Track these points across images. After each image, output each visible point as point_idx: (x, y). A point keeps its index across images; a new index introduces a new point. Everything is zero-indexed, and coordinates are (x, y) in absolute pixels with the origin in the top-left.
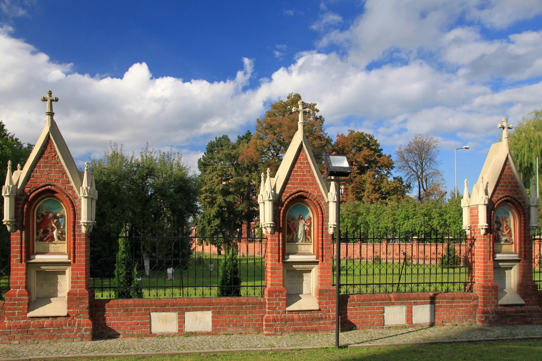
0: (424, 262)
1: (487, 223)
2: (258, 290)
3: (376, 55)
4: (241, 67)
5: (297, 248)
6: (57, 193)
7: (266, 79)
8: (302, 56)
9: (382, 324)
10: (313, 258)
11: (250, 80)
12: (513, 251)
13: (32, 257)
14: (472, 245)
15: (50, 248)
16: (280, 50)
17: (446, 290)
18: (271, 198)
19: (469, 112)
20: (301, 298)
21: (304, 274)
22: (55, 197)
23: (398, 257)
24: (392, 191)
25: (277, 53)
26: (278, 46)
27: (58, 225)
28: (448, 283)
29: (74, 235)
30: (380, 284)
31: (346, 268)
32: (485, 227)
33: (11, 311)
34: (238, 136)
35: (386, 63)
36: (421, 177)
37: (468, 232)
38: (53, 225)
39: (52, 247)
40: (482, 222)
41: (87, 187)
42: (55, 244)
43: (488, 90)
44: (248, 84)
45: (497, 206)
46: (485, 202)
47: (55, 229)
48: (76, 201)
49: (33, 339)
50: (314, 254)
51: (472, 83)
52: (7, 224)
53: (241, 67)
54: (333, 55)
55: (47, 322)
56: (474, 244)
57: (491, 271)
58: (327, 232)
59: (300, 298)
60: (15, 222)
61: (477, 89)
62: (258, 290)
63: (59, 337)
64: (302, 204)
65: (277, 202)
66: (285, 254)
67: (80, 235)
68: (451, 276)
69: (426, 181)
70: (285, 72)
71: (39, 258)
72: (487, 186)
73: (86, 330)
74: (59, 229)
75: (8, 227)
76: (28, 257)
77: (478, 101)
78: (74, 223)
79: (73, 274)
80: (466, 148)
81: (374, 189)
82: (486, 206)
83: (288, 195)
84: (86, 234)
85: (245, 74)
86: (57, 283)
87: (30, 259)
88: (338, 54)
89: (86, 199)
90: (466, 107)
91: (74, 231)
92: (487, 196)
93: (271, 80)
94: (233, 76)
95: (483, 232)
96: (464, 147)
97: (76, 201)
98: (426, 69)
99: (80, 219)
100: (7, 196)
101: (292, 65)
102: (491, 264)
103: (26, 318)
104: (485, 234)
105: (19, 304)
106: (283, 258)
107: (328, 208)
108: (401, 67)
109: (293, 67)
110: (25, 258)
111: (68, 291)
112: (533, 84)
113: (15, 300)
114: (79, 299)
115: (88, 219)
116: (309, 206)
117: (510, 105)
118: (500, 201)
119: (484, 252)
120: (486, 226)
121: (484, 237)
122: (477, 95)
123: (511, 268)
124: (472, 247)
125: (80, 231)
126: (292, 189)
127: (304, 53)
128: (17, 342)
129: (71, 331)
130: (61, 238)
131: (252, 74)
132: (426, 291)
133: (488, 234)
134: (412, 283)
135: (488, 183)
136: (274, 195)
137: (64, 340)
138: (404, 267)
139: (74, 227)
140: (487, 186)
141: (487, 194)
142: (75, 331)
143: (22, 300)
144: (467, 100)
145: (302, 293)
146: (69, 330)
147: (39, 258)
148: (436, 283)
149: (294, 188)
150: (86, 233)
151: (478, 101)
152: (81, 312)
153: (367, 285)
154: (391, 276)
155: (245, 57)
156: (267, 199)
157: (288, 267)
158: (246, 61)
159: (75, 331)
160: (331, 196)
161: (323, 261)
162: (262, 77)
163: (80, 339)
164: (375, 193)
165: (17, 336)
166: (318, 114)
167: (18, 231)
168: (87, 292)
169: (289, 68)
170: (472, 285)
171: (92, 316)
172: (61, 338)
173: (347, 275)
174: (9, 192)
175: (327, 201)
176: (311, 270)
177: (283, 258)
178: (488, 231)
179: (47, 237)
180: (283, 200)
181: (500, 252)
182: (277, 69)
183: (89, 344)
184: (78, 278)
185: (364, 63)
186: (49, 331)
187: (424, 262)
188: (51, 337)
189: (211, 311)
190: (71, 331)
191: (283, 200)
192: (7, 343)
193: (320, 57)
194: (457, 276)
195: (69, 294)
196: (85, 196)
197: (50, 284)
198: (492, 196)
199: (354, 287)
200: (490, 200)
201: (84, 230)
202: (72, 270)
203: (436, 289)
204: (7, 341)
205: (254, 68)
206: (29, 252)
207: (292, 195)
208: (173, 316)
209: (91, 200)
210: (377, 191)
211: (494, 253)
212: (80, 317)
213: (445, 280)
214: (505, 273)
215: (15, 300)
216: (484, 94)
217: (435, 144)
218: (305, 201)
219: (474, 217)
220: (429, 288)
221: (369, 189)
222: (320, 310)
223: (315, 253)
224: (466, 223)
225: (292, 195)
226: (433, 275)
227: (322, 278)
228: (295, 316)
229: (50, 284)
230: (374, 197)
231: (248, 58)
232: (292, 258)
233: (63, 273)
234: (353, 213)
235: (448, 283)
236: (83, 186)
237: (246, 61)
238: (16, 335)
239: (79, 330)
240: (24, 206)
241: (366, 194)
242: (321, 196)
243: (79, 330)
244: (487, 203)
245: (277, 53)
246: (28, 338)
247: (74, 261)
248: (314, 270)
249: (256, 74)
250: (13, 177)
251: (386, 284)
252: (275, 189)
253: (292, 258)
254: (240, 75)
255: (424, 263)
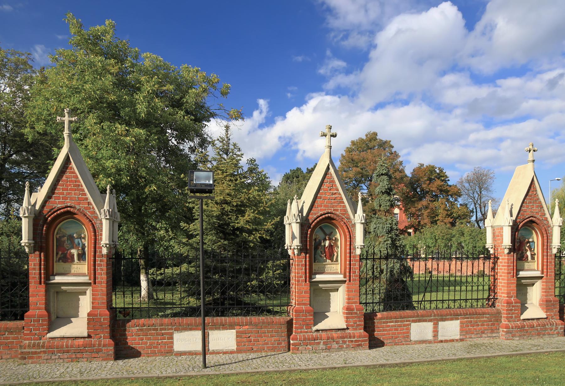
0: (472, 279)
1: (511, 243)
2: (446, 303)
3: (381, 97)
4: (257, 107)
5: (324, 268)
6: (76, 214)
7: (280, 118)
8: (311, 98)
9: (169, 351)
10: (340, 277)
11: (266, 118)
12: (536, 268)
13: (51, 277)
14: (495, 263)
15: (525, 266)
16: (291, 92)
17: (481, 306)
18: (299, 221)
19: (466, 146)
20: (527, 308)
21: (80, 297)
22: (74, 218)
23: (448, 274)
24: (463, 215)
25: (289, 95)
26: (290, 89)
27: (530, 248)
28: (472, 299)
29: (95, 256)
30: (477, 299)
31: (477, 284)
32: (508, 247)
33: (383, 321)
34: (307, 168)
35: (389, 103)
36: (479, 202)
37: (492, 251)
38: (527, 248)
39: (526, 265)
40: (507, 241)
41: (27, 206)
42: (529, 262)
43: (480, 126)
44: (264, 122)
45: (522, 227)
46: (297, 220)
47: (527, 251)
48: (549, 229)
49: (527, 336)
50: (341, 273)
51: (466, 121)
52: (25, 245)
53: (257, 107)
54: (345, 98)
55: (535, 323)
56: (497, 262)
57: (514, 287)
58: (551, 252)
59: (327, 317)
60: (34, 243)
61: (471, 126)
62: (446, 303)
63: (544, 335)
64: (529, 228)
65: (304, 224)
66: (312, 273)
67: (551, 255)
68: (463, 294)
69: (485, 207)
70: (298, 110)
71: (58, 279)
72: (512, 208)
73: (561, 328)
74: (531, 250)
75: (26, 248)
76: (47, 278)
77: (472, 137)
78: (95, 243)
79: (93, 295)
80: (558, 180)
81: (447, 214)
82: (510, 228)
83: (315, 216)
84: (107, 255)
85: (261, 112)
86: (527, 293)
87: (50, 280)
88: (349, 96)
89: (27, 219)
90: (463, 142)
91: (95, 252)
92: (512, 218)
93: (285, 117)
94: (250, 115)
95: (506, 251)
96: (556, 179)
97: (549, 229)
98: (425, 108)
99: (101, 239)
100: (25, 217)
101: (304, 106)
102: (514, 280)
103: (519, 320)
104: (509, 253)
105: (515, 310)
106: (311, 278)
107: (355, 229)
108: (402, 106)
109: (304, 107)
110: (44, 279)
111: (89, 311)
112: (522, 122)
113: (513, 306)
114: (553, 305)
115: (28, 240)
116: (338, 228)
117: (501, 140)
118: (324, 216)
119: (508, 270)
120: (509, 246)
121: (508, 256)
122: (473, 131)
123: (533, 285)
124: (495, 265)
125: (101, 252)
126: (318, 211)
127: (314, 95)
128: (518, 338)
129: (551, 329)
130: (81, 257)
131: (268, 112)
132: (439, 308)
133: (512, 253)
134: (472, 299)
135: (512, 205)
136: (302, 218)
137: (547, 336)
138: (426, 284)
139: (95, 248)
140: (512, 208)
141: (511, 216)
142: (554, 329)
143: (517, 306)
144: (464, 135)
145: (527, 304)
146: (550, 328)
147: (58, 279)
148: (460, 300)
149: (59, 203)
150: (107, 255)
151: (472, 137)
152: (555, 315)
153: (443, 301)
154: (470, 293)
155: (261, 98)
156: (359, 221)
157: (314, 285)
158: (262, 102)
159: (554, 329)
160: (359, 217)
161: (350, 281)
162: (277, 116)
163: (557, 335)
164: (448, 217)
165: (517, 334)
166: (393, 150)
167: (512, 253)
168: (108, 313)
169: (302, 108)
170: (494, 301)
171: (113, 336)
172: (545, 335)
173: (449, 291)
174: (28, 213)
175: (100, 219)
176: (338, 289)
177: (311, 278)
178: (512, 250)
179: (67, 259)
180: (311, 221)
181: (523, 270)
182: (290, 109)
183: (369, 351)
184: (550, 289)
185: (370, 104)
186: (537, 330)
187: (472, 279)
188: (539, 334)
189: (459, 321)
190: (551, 329)
191: (311, 221)
192: (511, 339)
193: (328, 98)
194: (458, 293)
195: (89, 315)
196: (107, 217)
197: (523, 294)
198: (516, 219)
199: (443, 303)
200: (515, 222)
201: (105, 251)
202: (93, 291)
203: (472, 305)
204: (511, 338)
205: (269, 107)
206: (49, 273)
207: (319, 217)
208: (429, 326)
209: (113, 222)
210: (449, 215)
211: (518, 271)
212: (554, 318)
213: (457, 297)
214: (330, 295)
215: (513, 306)
216: (477, 131)
217: (491, 175)
218: (333, 223)
219: (497, 236)
220: (465, 304)
221: (442, 214)
222: (547, 318)
223: (540, 269)
224: (489, 243)
225: (319, 217)
226: (446, 293)
227: (546, 291)
228: (324, 334)
229: (523, 294)
230: (448, 221)
231: (263, 99)
232: (319, 277)
233: (84, 293)
234: (446, 235)
235: (460, 300)
236: (105, 208)
237: (262, 102)
238: (517, 334)
239: (556, 329)
240: (43, 227)
241: (440, 217)
242: (349, 218)
243: (556, 329)
244: (511, 224)
245: (289, 95)
246: (524, 335)
247: (95, 283)
248: (341, 289)
249: (271, 112)
250: (31, 199)
251: (449, 300)
252: (301, 211)
253: (319, 277)
254: (256, 114)
255: (472, 280)
